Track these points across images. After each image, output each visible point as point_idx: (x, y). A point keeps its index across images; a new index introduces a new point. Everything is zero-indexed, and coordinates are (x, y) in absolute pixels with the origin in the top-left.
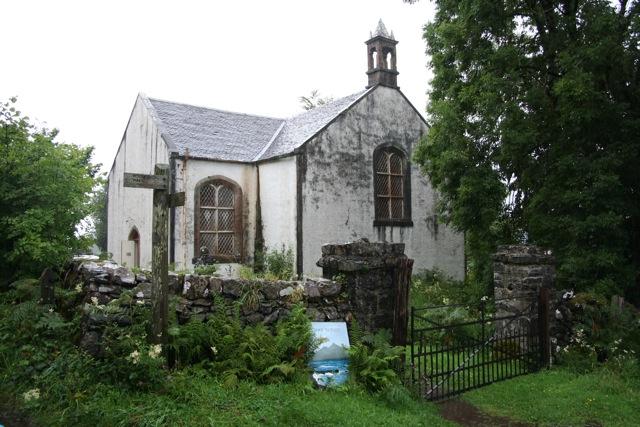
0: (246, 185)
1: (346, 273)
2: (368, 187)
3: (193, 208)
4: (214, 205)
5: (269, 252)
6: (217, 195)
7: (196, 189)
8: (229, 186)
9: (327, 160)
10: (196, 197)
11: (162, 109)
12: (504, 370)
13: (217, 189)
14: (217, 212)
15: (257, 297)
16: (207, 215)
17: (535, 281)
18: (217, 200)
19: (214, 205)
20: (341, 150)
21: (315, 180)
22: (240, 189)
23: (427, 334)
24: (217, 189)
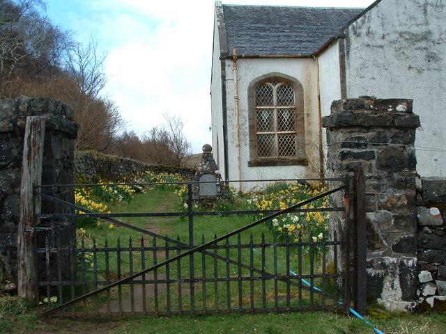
0: (309, 81)
1: (417, 194)
2: (439, 70)
3: (247, 109)
4: (272, 104)
5: (196, 132)
6: (275, 93)
7: (250, 89)
8: (288, 84)
9: (380, 42)
10: (250, 96)
11: (225, 7)
12: (174, 297)
13: (275, 88)
14: (275, 112)
15: (15, 152)
16: (265, 116)
17: (356, 156)
18: (275, 98)
19: (272, 104)
20: (399, 29)
21: (364, 66)
22: (301, 85)
23: (233, 241)
24: (275, 88)
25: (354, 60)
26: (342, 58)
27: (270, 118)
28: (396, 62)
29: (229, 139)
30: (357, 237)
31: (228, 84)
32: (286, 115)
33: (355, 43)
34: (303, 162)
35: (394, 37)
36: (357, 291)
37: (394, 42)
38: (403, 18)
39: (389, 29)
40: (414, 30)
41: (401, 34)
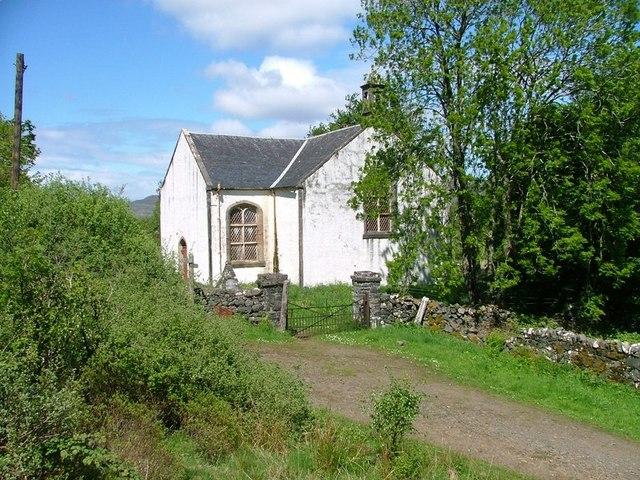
4: (240, 222)
8: (253, 208)
9: (323, 190)
20: (335, 181)
21: (313, 206)
25: (308, 203)
26: (300, 202)
27: (240, 233)
28: (333, 204)
29: (213, 248)
30: (365, 310)
31: (213, 208)
32: (250, 230)
33: (309, 191)
34: (262, 265)
35: (332, 187)
36: (365, 324)
37: (332, 190)
38: (338, 174)
39: (329, 181)
40: (344, 182)
41: (337, 185)
